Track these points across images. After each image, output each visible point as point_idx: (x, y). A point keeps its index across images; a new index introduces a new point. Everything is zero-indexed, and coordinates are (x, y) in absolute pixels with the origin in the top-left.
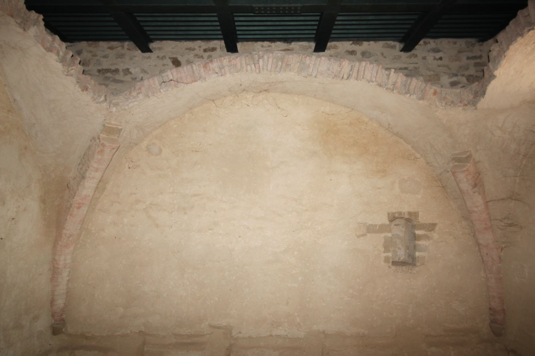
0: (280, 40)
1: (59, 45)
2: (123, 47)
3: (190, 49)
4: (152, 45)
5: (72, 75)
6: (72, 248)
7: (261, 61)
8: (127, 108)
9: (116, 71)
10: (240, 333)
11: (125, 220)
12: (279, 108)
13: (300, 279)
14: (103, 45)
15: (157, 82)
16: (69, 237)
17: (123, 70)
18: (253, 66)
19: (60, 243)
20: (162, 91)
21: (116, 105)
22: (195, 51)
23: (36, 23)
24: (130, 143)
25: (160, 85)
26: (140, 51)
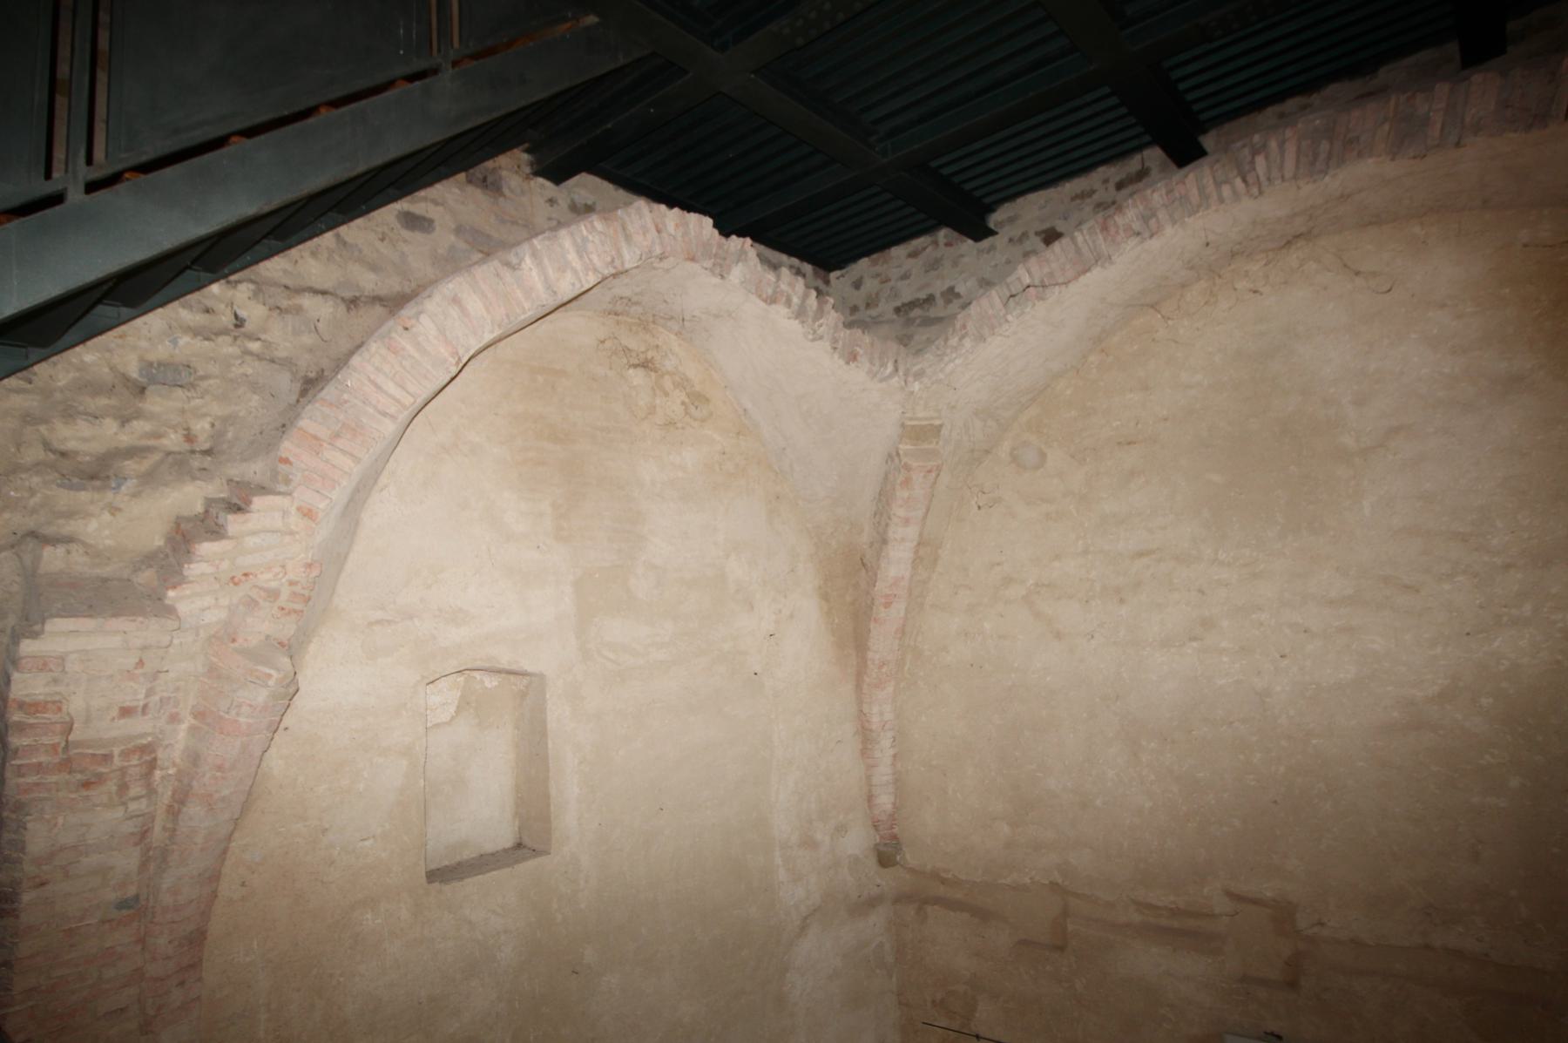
0: (1334, 77)
1: (790, 284)
2: (936, 243)
3: (1083, 196)
4: (994, 219)
5: (821, 338)
6: (890, 689)
7: (1260, 161)
8: (941, 376)
9: (930, 299)
10: (1321, 924)
11: (987, 625)
12: (1357, 273)
13: (1515, 782)
14: (898, 252)
15: (997, 301)
16: (880, 667)
17: (943, 294)
18: (1238, 181)
19: (867, 679)
20: (1010, 317)
21: (919, 375)
22: (1096, 197)
23: (741, 256)
24: (972, 451)
25: (1005, 305)
26: (970, 242)
